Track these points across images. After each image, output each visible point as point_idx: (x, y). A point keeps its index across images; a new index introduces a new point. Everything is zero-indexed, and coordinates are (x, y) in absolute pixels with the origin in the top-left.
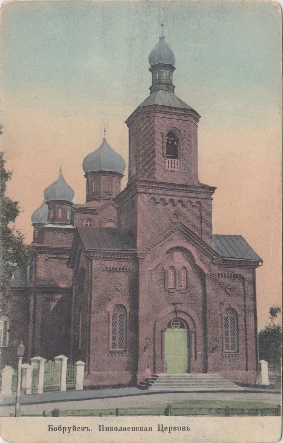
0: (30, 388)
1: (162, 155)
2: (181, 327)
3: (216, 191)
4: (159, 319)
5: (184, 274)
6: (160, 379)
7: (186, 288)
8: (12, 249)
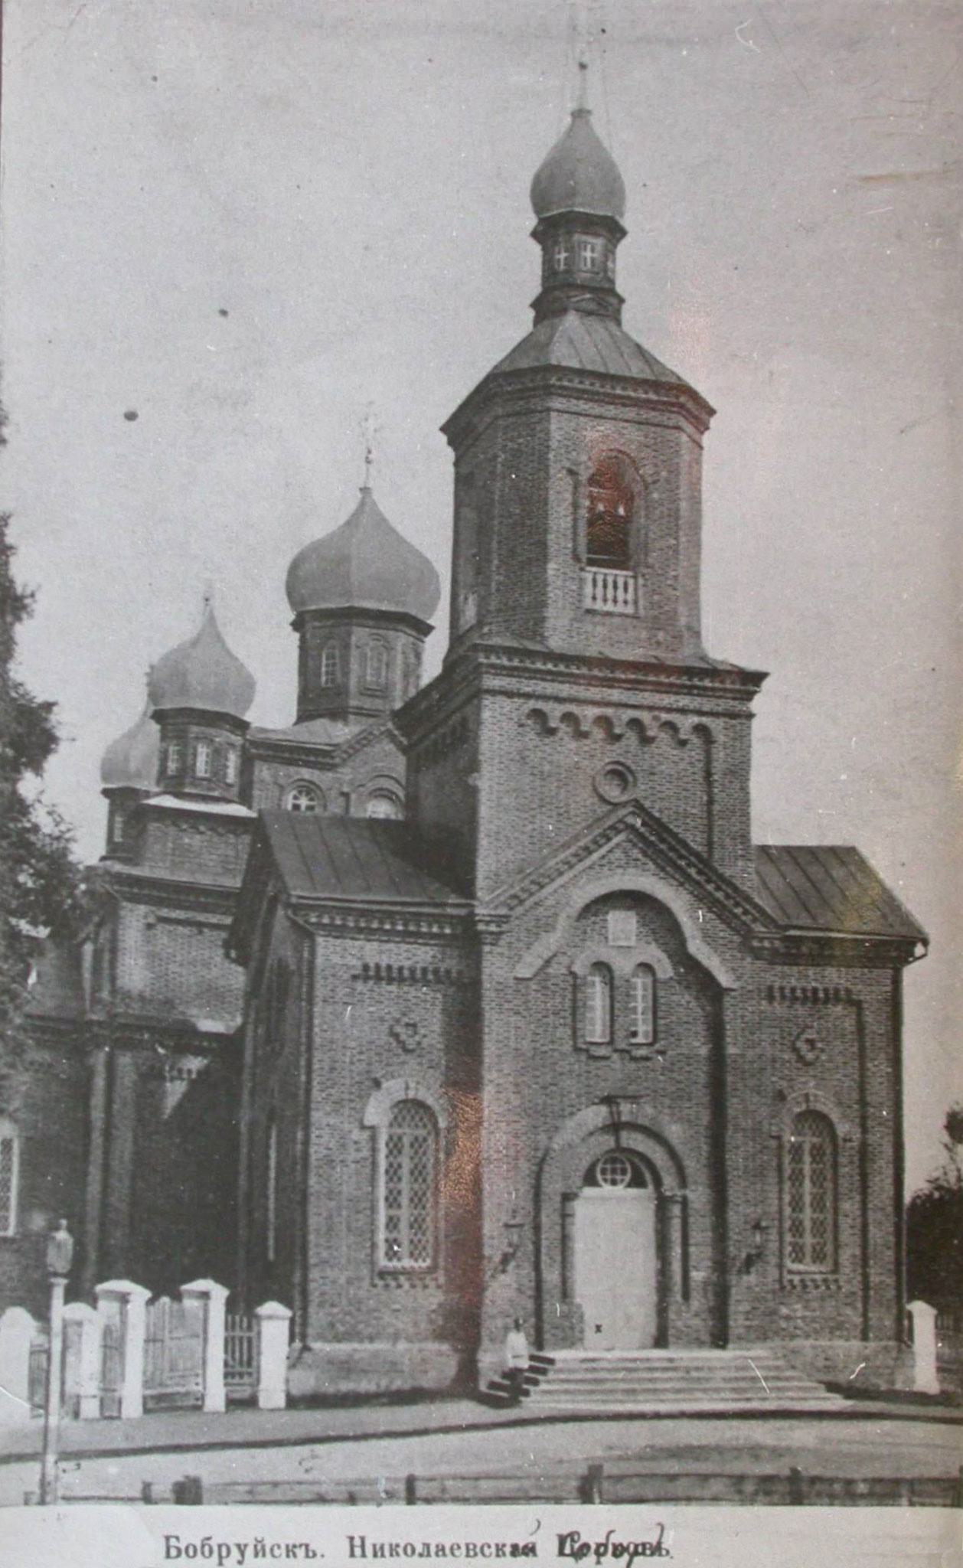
0: (94, 1397)
1: (571, 556)
2: (629, 1185)
3: (766, 684)
4: (553, 1154)
5: (645, 989)
6: (561, 1371)
7: (650, 1040)
8: (32, 875)
